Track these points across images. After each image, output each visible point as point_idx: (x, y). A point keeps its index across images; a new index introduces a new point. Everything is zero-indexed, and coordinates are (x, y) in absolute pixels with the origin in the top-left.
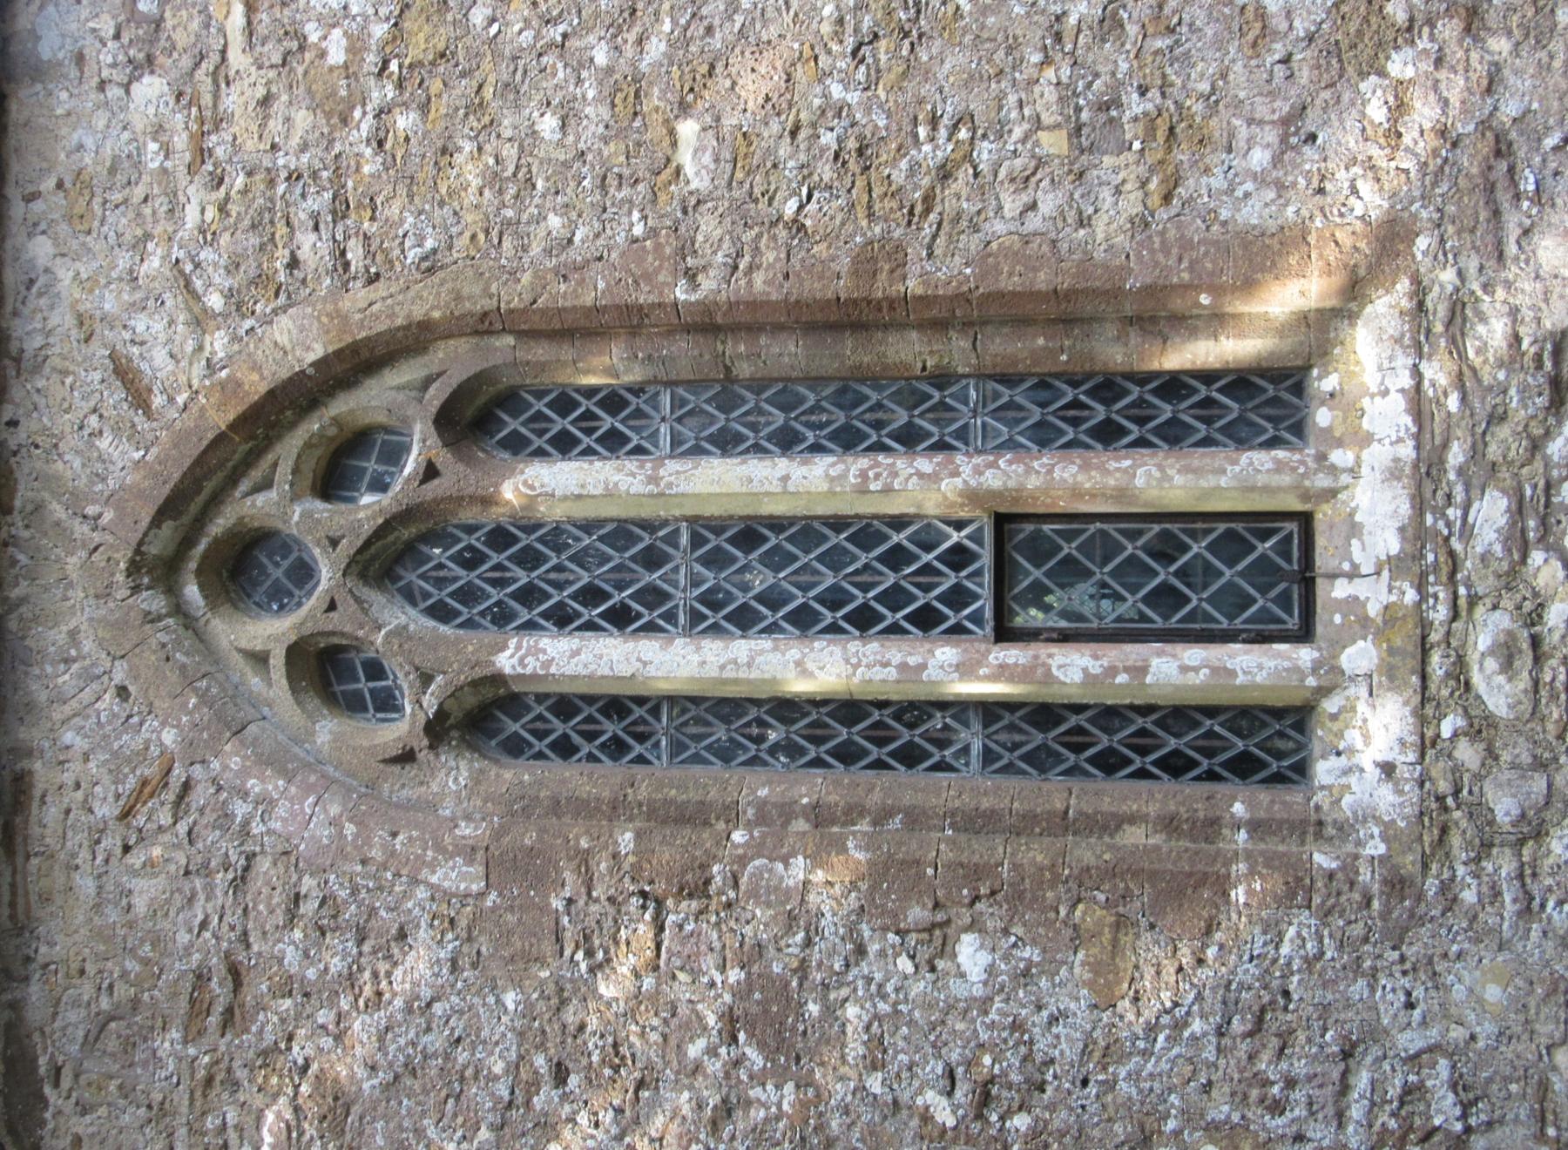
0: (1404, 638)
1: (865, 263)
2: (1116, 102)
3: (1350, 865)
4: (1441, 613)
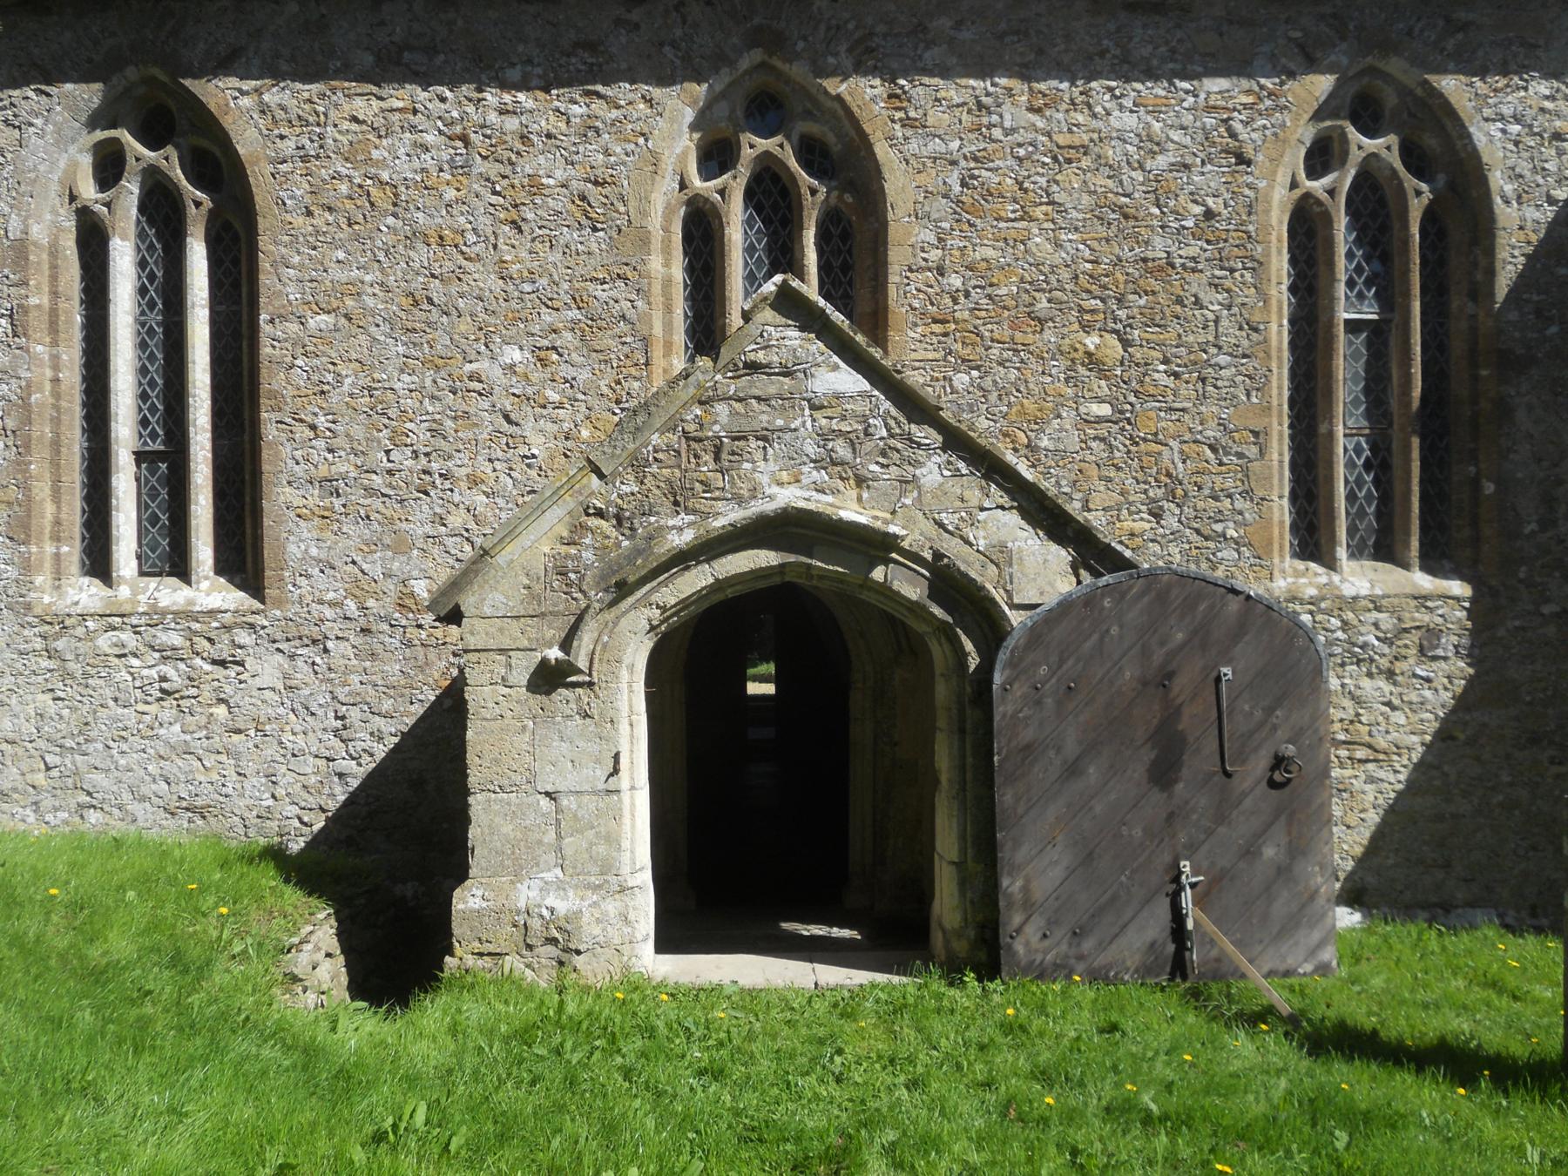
0: (127, 608)
1: (274, 395)
2: (338, 495)
3: (36, 589)
4: (135, 621)
